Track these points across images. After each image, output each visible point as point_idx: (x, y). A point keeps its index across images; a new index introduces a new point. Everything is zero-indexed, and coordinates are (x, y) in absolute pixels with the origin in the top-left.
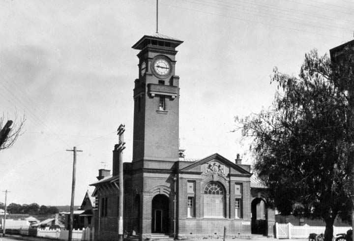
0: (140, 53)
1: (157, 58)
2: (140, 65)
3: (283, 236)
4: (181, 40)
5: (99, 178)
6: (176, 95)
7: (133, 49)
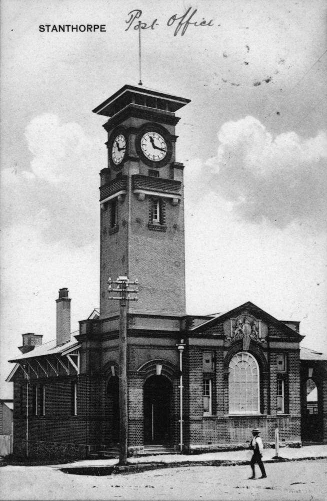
0: (109, 121)
2: (110, 145)
5: (25, 348)
6: (179, 197)
7: (95, 114)
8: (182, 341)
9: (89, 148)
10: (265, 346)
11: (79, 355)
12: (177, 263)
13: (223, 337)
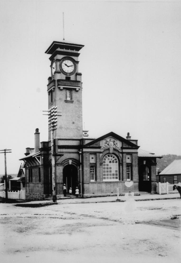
1: (64, 59)
2: (51, 66)
3: (164, 192)
4: (83, 45)
6: (79, 88)
7: (46, 54)
8: (81, 150)
9: (44, 69)
10: (120, 151)
11: (40, 157)
12: (79, 116)
13: (99, 148)
